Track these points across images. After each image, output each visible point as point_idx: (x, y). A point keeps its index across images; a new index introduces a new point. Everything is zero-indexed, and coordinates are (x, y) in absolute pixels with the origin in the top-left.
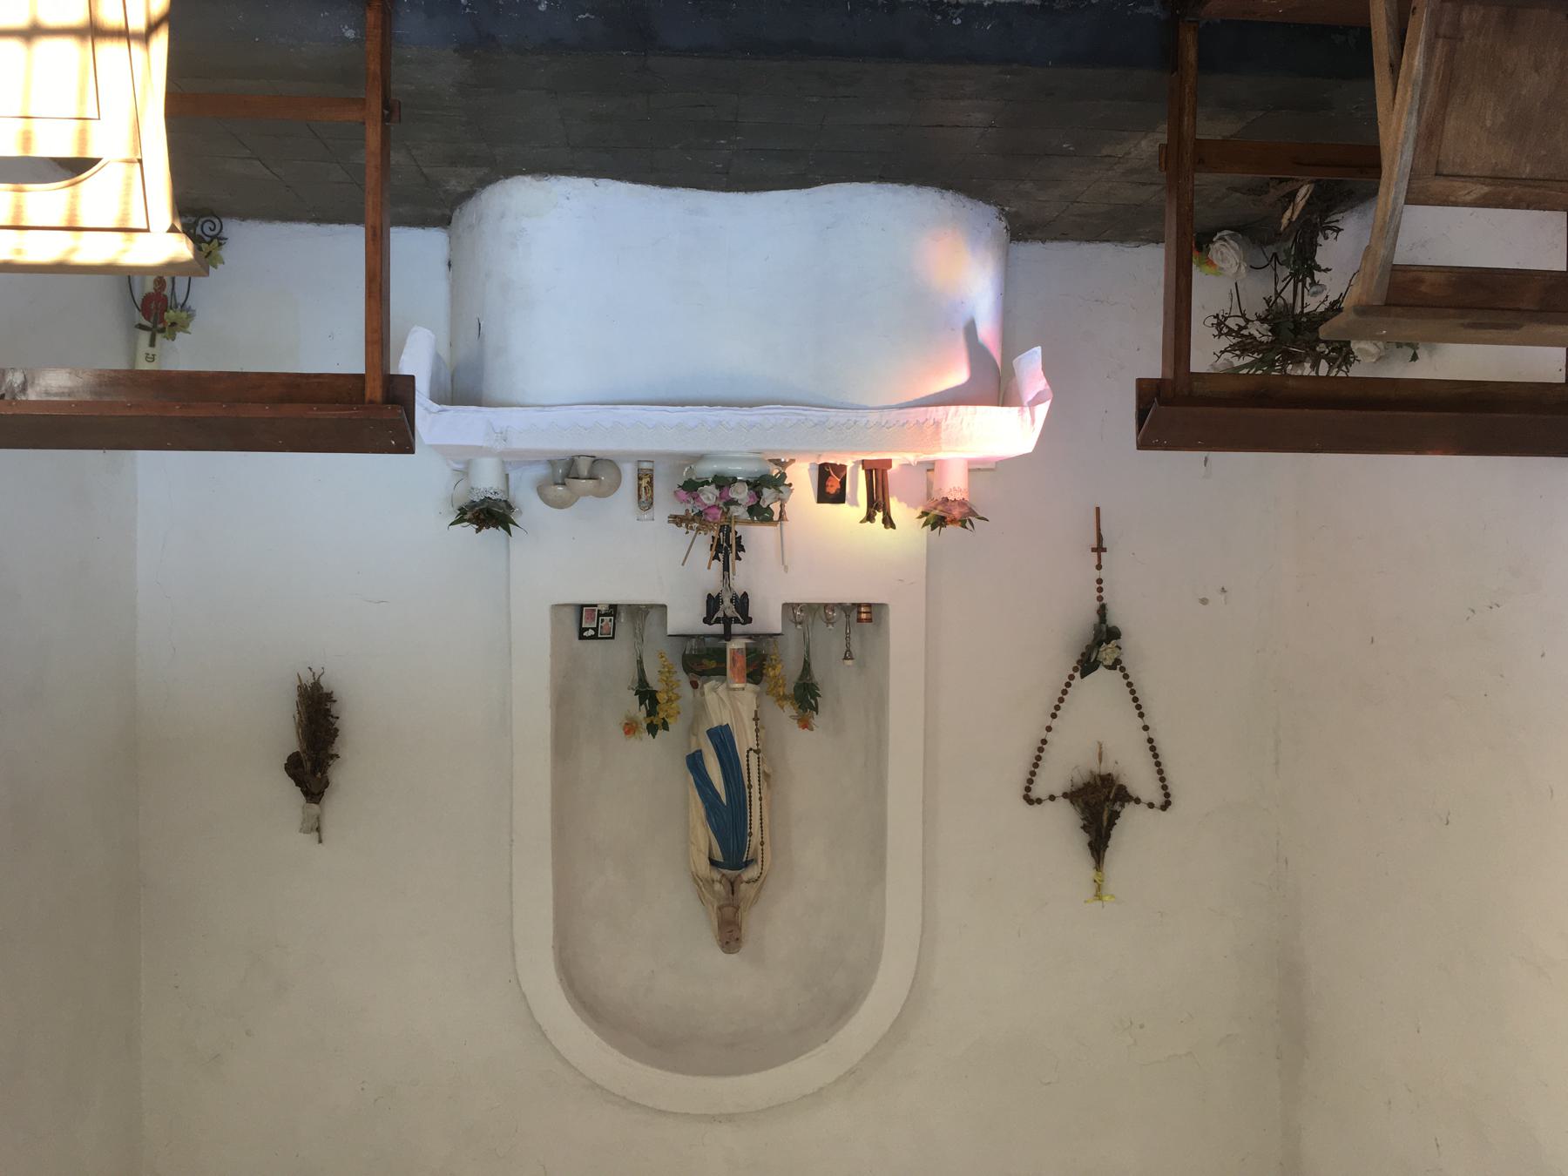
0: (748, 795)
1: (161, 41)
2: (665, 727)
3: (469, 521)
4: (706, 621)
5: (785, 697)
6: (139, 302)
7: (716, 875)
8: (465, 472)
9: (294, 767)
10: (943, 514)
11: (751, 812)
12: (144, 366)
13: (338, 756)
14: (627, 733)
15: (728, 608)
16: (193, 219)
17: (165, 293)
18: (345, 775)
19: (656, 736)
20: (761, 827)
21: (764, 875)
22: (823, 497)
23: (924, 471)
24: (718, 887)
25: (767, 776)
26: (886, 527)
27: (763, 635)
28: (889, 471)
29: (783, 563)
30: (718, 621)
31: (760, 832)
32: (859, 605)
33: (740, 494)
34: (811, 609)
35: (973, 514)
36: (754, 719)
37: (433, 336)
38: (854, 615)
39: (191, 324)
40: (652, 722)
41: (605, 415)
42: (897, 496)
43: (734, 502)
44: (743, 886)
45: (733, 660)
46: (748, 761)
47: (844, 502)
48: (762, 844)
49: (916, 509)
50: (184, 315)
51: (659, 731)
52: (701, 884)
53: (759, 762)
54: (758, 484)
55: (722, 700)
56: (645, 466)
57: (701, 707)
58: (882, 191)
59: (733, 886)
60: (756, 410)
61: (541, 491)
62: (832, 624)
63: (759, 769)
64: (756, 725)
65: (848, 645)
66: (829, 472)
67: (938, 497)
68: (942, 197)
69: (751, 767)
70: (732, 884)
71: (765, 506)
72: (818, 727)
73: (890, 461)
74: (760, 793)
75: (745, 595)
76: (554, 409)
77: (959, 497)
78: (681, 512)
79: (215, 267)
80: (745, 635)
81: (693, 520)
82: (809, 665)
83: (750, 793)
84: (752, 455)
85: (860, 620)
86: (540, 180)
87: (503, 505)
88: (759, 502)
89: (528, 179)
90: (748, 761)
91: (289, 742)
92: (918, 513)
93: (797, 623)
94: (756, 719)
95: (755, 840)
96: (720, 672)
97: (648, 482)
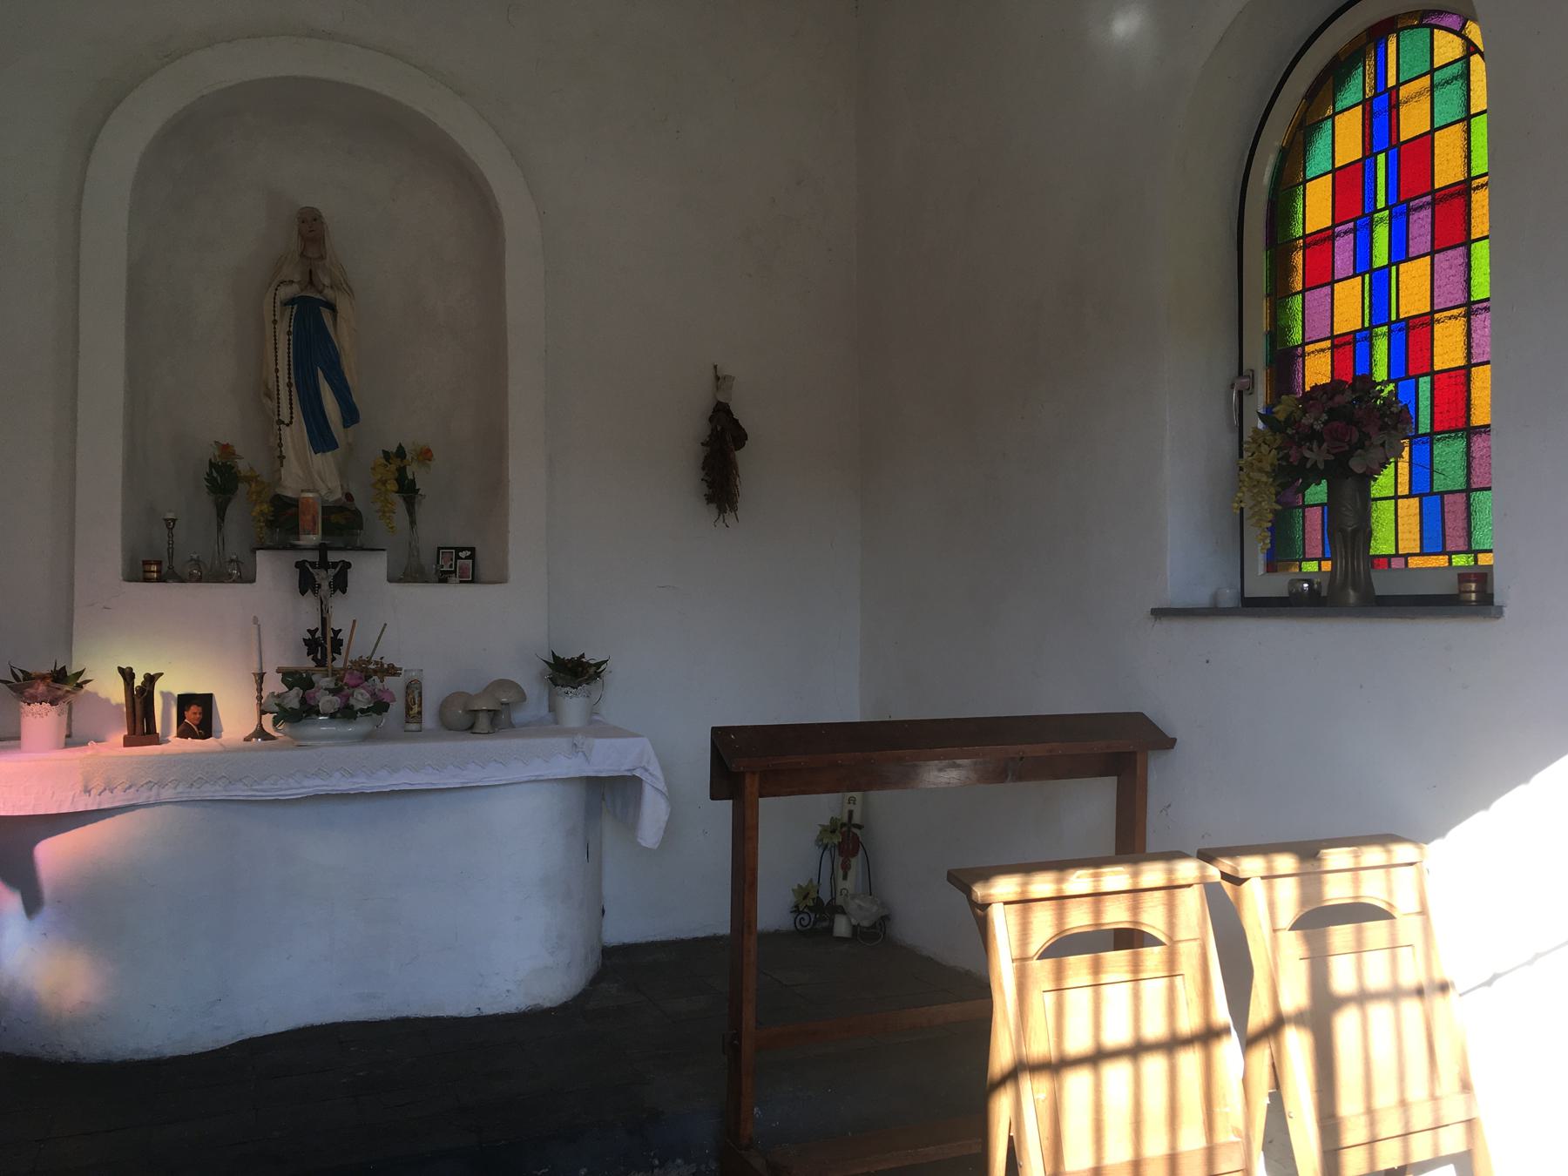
0: (292, 376)
1: (1002, 1055)
2: (387, 455)
3: (591, 665)
4: (349, 565)
5: (248, 480)
6: (861, 852)
7: (329, 294)
8: (593, 711)
9: (740, 437)
10: (57, 685)
11: (289, 357)
12: (857, 795)
13: (702, 444)
14: (429, 451)
15: (324, 578)
16: (817, 926)
17: (841, 859)
18: (691, 428)
19: (398, 445)
20: (275, 340)
21: (272, 289)
22: (206, 701)
23: (74, 735)
24: (327, 281)
25: (268, 395)
26: (131, 669)
27: (278, 549)
28: (126, 733)
29: (259, 626)
30: (335, 565)
31: (277, 334)
32: (160, 580)
33: (328, 701)
34: (217, 575)
35: (13, 688)
36: (284, 457)
37: (639, 840)
38: (165, 568)
39: (818, 833)
40: (402, 461)
41: (472, 776)
42: (112, 705)
43: (334, 692)
44: (297, 278)
45: (315, 523)
46: (292, 413)
47: (180, 696)
48: (275, 322)
49: (87, 692)
50: (825, 841)
51: (395, 451)
52: (344, 286)
53: (279, 411)
54: (306, 711)
55: (321, 478)
56: (413, 727)
57: (343, 474)
58: (155, 1050)
59: (311, 280)
60: (310, 791)
61: (523, 697)
62: (192, 560)
63: (279, 403)
64: (281, 451)
65: (170, 536)
66: (199, 729)
67: (63, 706)
68: (75, 1053)
69: (287, 403)
70: (311, 282)
71: (296, 689)
72: (211, 445)
73: (125, 745)
74: (277, 377)
75: (303, 592)
76: (526, 779)
77: (36, 707)
78: (387, 679)
79: (799, 886)
80: (301, 549)
81: (375, 672)
82: (218, 515)
83: (289, 378)
84: (309, 743)
85: (159, 563)
86: (535, 1005)
87: (559, 682)
88: (304, 694)
89: (547, 1004)
90: (292, 413)
91: (746, 460)
92: (87, 687)
93: (237, 561)
94: (282, 457)
95: (283, 327)
96: (327, 510)
97: (412, 709)
